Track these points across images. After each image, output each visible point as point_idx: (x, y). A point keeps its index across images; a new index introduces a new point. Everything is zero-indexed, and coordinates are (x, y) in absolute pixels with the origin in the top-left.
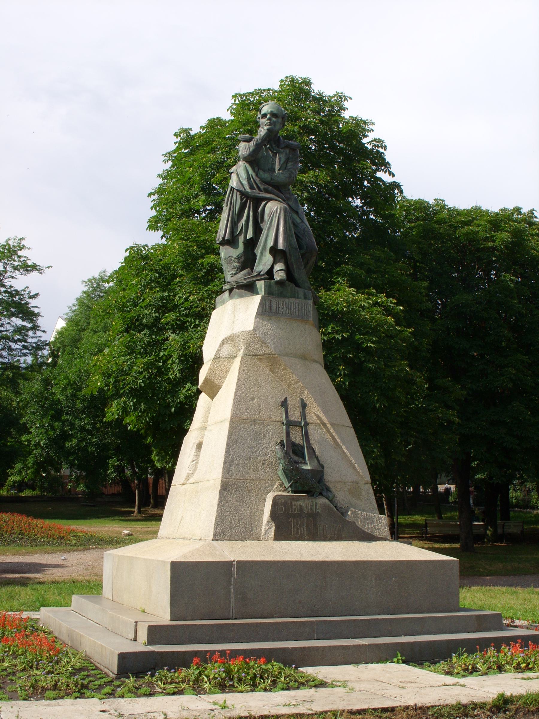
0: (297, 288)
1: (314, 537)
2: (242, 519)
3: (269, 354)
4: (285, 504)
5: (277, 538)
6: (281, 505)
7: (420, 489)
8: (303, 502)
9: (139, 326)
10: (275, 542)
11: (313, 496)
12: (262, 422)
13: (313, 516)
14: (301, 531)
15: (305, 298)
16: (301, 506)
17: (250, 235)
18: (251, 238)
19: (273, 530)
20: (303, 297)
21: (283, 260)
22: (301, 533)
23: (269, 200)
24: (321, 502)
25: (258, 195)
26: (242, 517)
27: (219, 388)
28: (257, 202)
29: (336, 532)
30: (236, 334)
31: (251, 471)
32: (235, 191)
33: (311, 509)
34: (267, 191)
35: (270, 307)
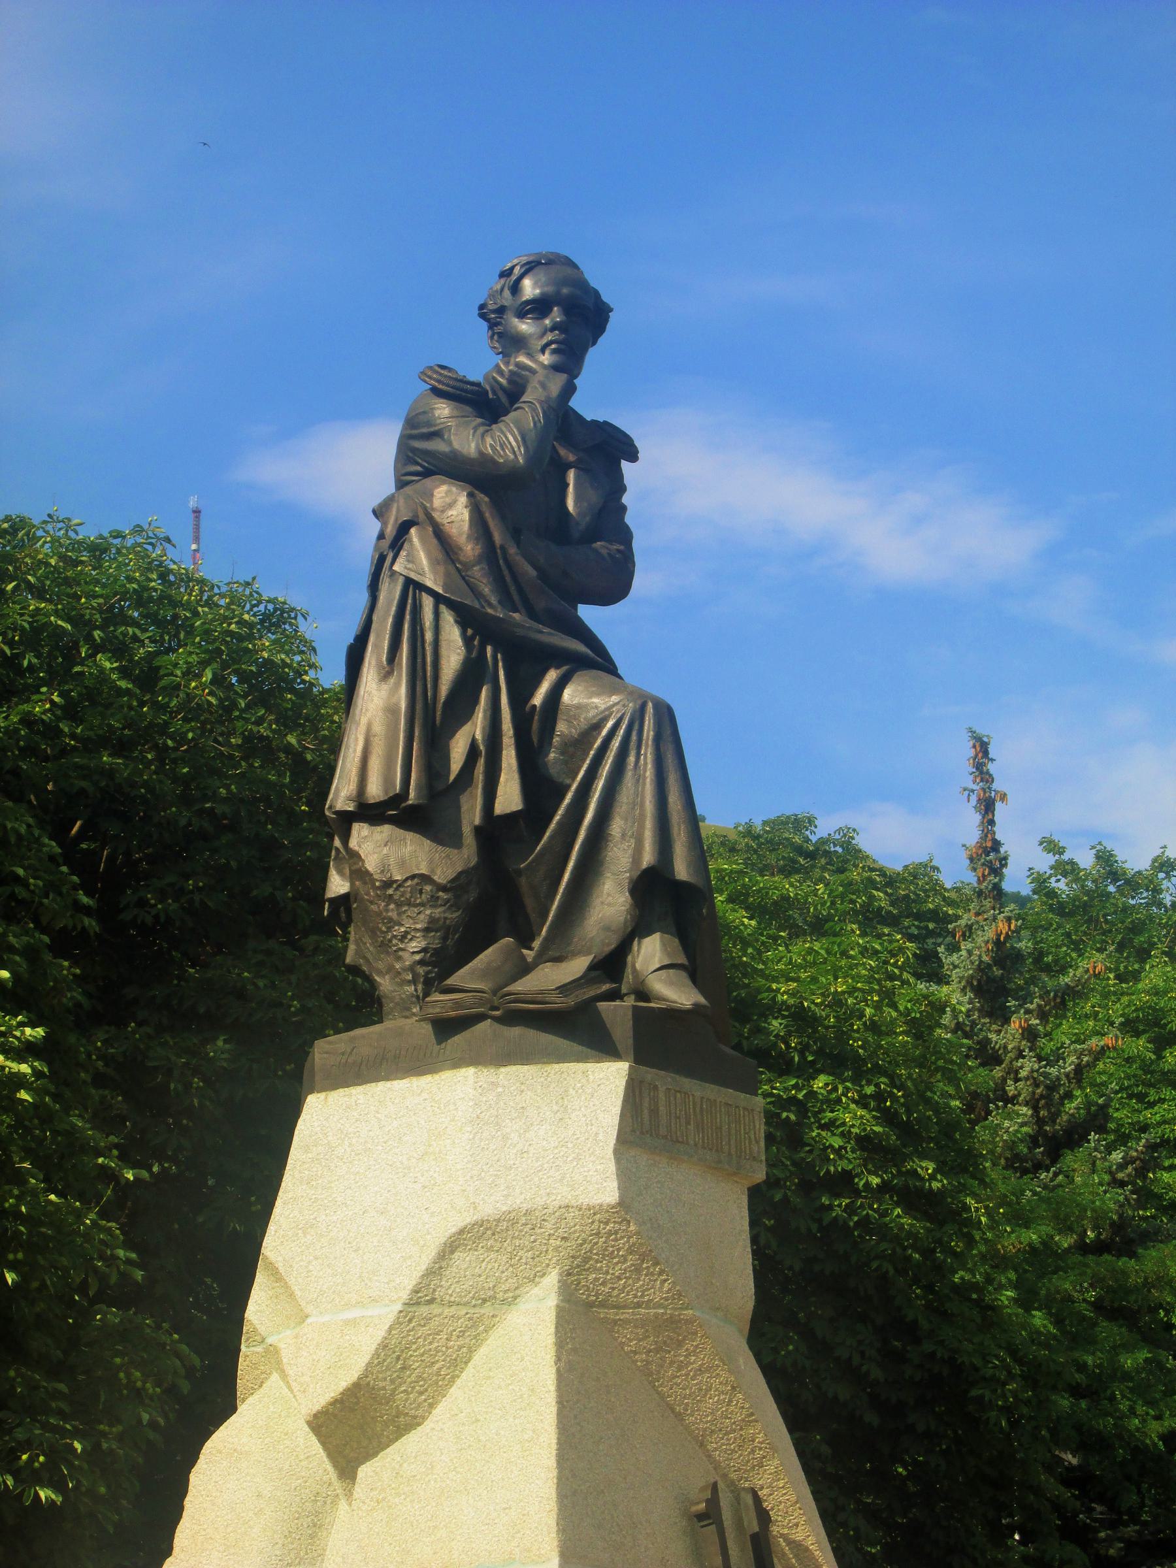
18: (511, 818)
25: (539, 637)
27: (413, 1423)
30: (528, 1213)
32: (428, 602)
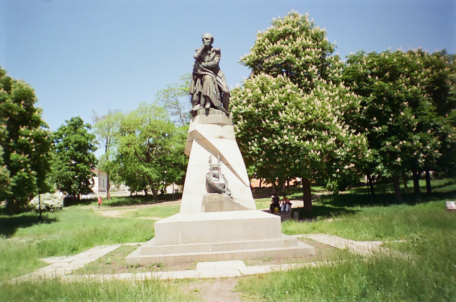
13: (221, 202)
19: (204, 208)
23: (206, 75)
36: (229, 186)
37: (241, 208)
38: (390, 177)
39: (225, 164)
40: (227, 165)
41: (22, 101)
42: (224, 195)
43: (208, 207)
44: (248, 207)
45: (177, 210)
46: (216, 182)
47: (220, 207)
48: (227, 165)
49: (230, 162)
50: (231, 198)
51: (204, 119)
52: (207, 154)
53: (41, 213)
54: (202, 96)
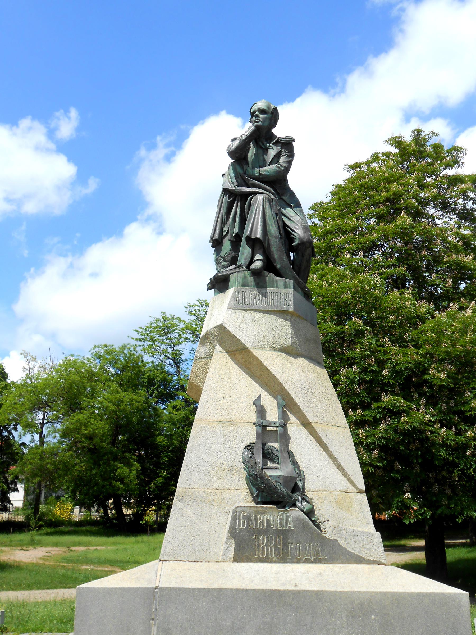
0: (277, 278)
1: (284, 557)
2: (198, 535)
3: (242, 349)
4: (248, 518)
5: (237, 559)
6: (243, 518)
7: (122, 512)
8: (272, 515)
9: (355, 299)
10: (236, 564)
11: (284, 507)
12: (233, 423)
13: (284, 533)
14: (267, 550)
15: (286, 286)
16: (268, 520)
17: (236, 230)
19: (232, 549)
20: (283, 287)
21: (261, 251)
22: (268, 554)
23: (256, 193)
24: (294, 515)
25: (244, 190)
26: (199, 533)
28: (244, 197)
29: (312, 552)
31: (215, 479)
33: (281, 524)
34: (254, 186)
35: (244, 299)
36: (311, 486)
37: (326, 550)
38: (168, 497)
39: (303, 425)
40: (306, 424)
41: (133, 499)
42: (295, 513)
43: (246, 544)
44: (363, 555)
45: (153, 554)
46: (276, 472)
47: (284, 548)
48: (306, 424)
49: (310, 417)
50: (313, 522)
51: (244, 299)
52: (249, 389)
53: (435, 482)
54: (244, 240)
